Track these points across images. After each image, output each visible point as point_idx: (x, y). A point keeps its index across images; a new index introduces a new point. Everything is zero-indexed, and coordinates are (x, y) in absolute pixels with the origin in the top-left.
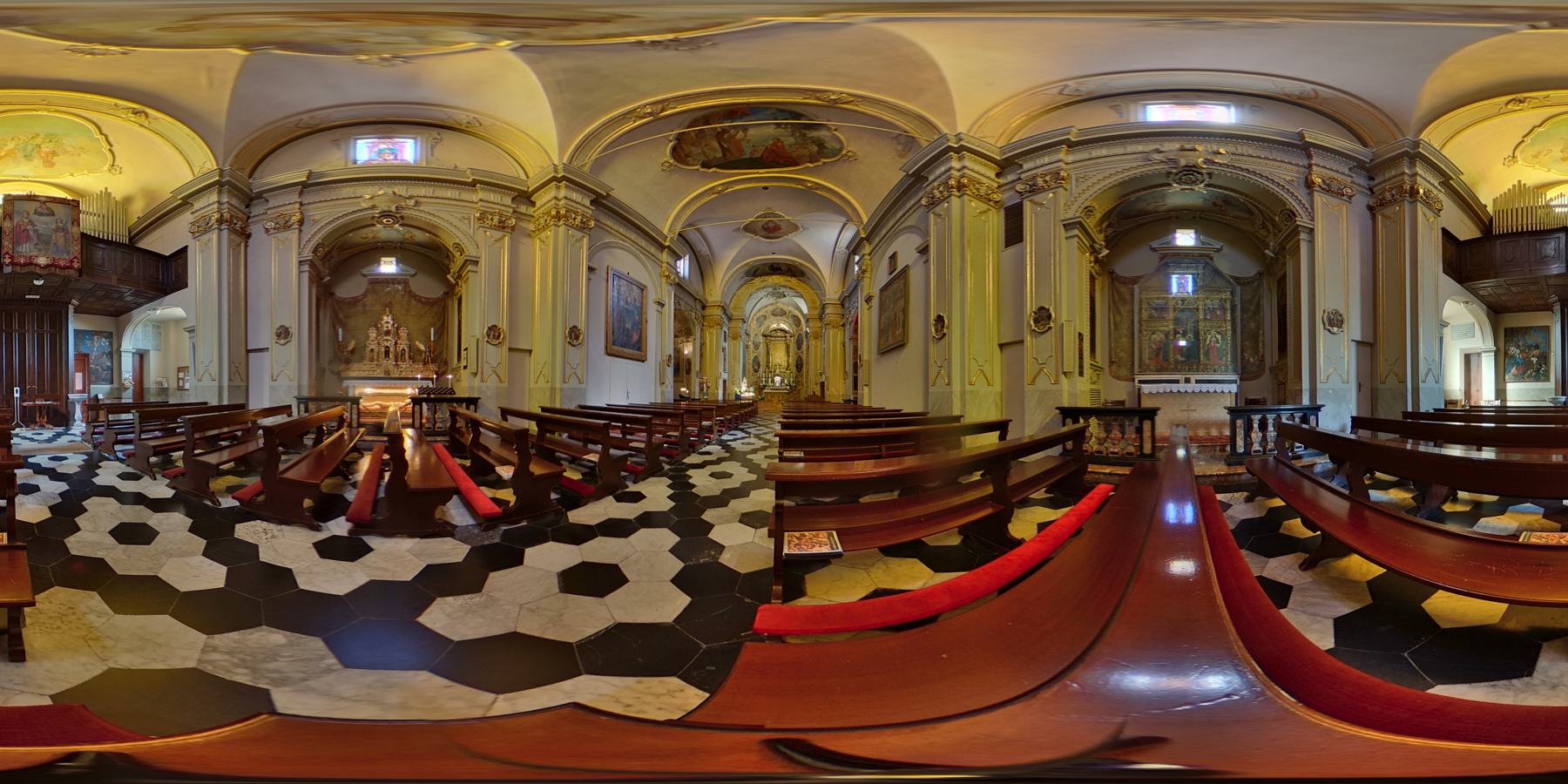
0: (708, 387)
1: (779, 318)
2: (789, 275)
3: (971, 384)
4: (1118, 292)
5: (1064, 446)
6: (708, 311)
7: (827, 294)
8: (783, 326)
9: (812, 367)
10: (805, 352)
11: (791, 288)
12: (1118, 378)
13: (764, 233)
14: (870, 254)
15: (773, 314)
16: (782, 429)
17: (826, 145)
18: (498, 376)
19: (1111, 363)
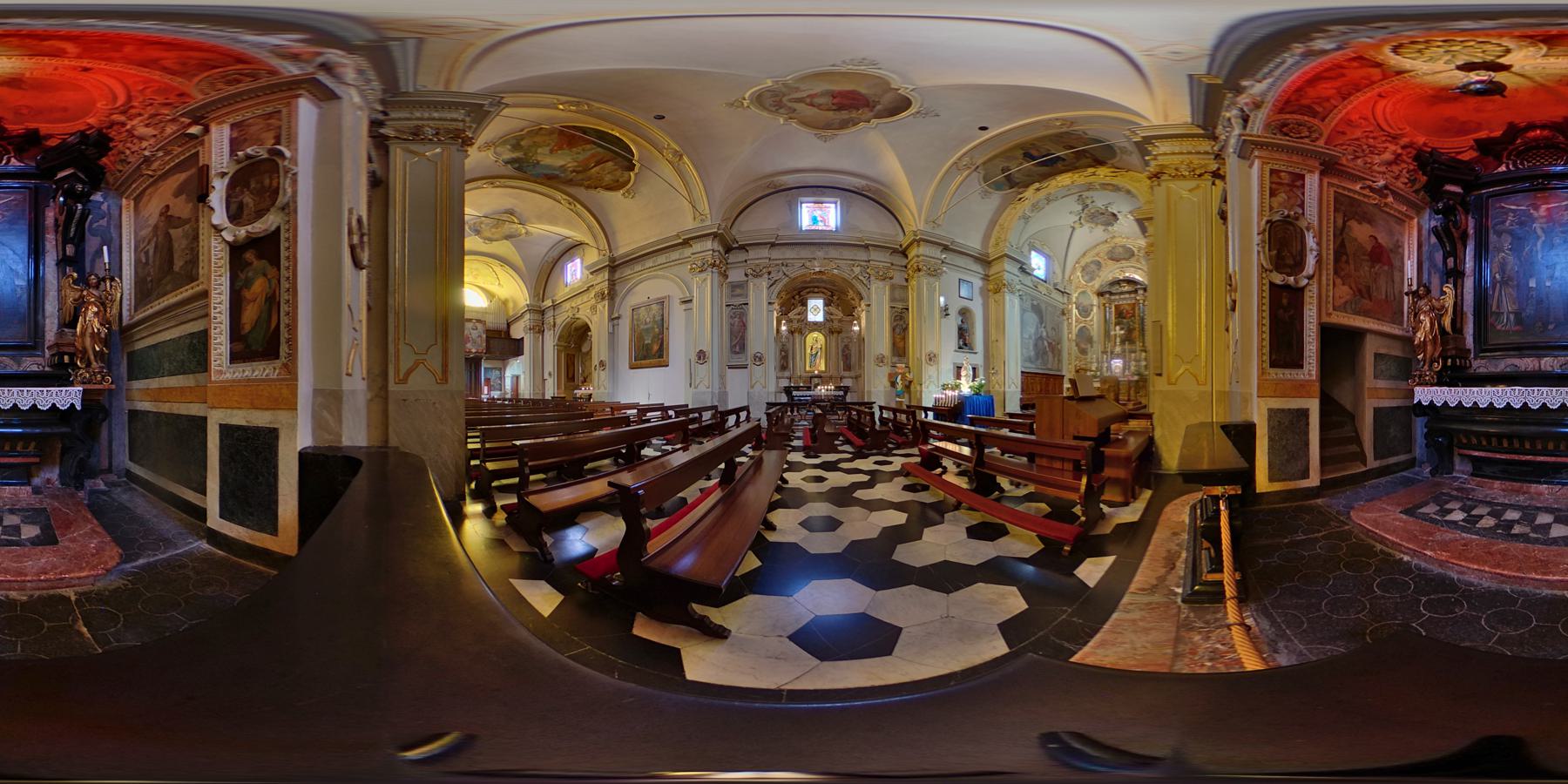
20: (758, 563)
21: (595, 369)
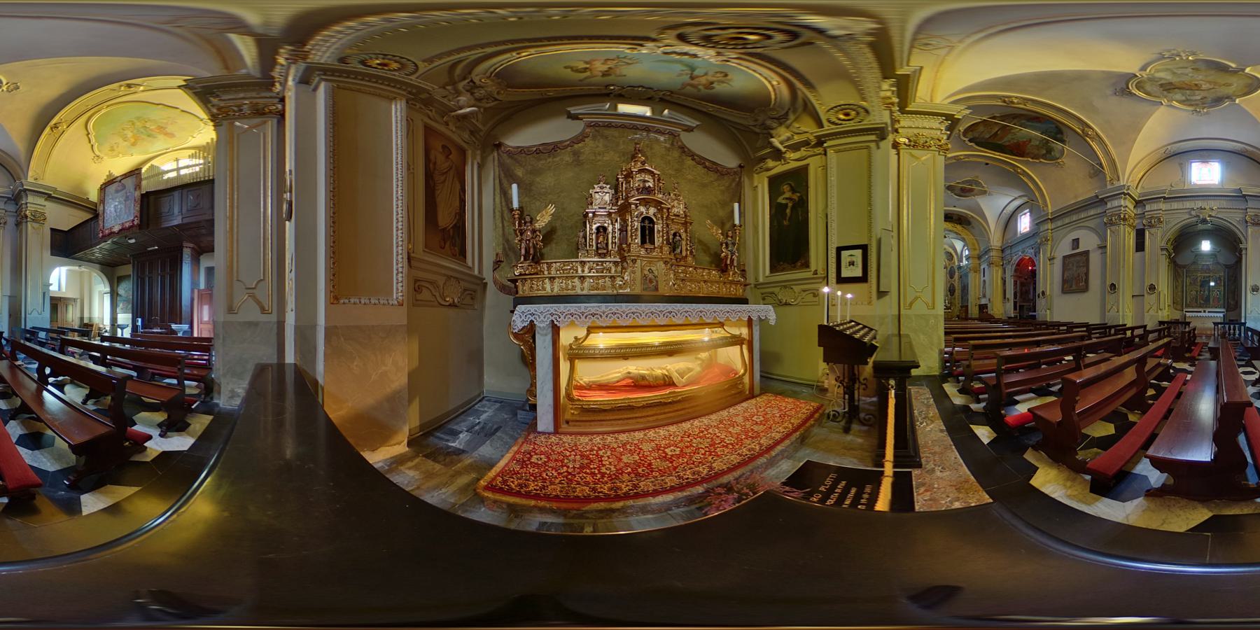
4: (1178, 272)
5: (178, 164)
7: (992, 242)
12: (1176, 309)
14: (1052, 230)
18: (259, 303)
19: (1174, 303)
20: (986, 441)
21: (1039, 297)
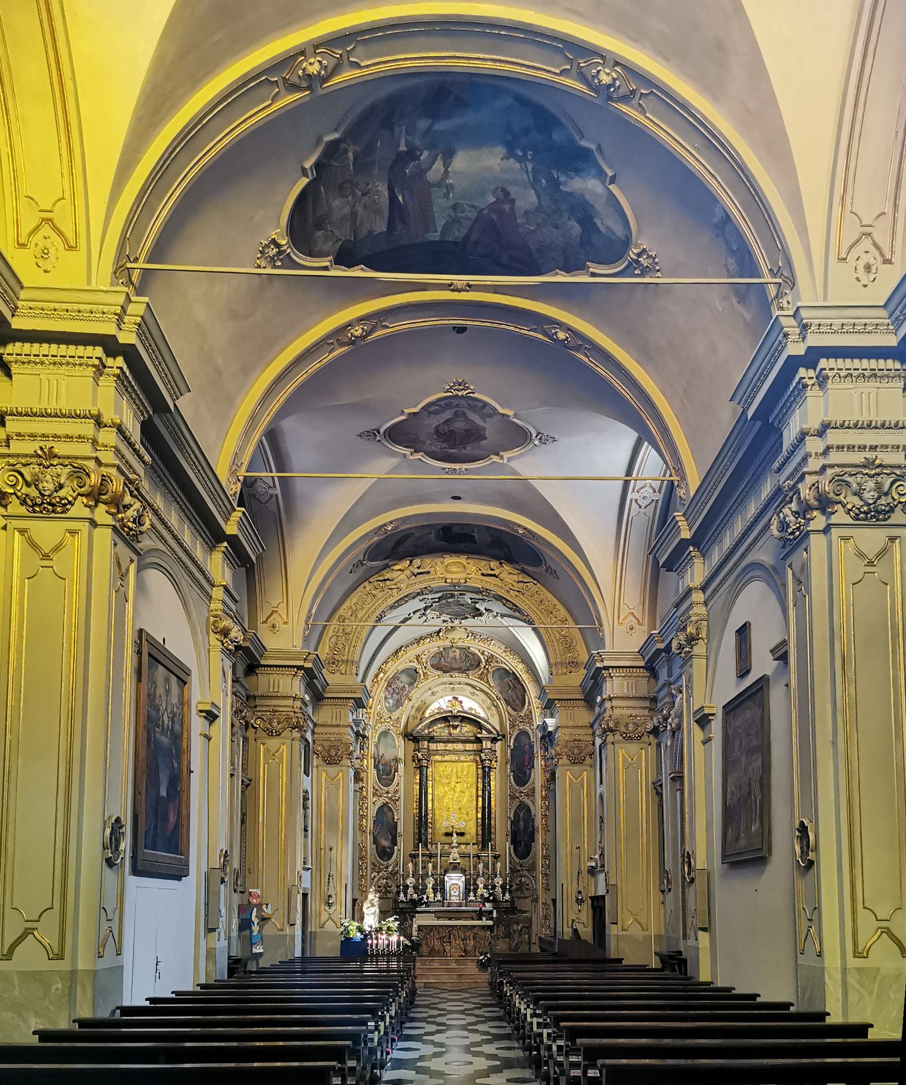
0: (264, 920)
1: (459, 677)
2: (496, 558)
3: (857, 955)
6: (264, 682)
8: (472, 705)
9: (564, 850)
10: (539, 793)
11: (499, 598)
13: (437, 447)
15: (437, 667)
16: (40, 1041)
17: (598, 222)
